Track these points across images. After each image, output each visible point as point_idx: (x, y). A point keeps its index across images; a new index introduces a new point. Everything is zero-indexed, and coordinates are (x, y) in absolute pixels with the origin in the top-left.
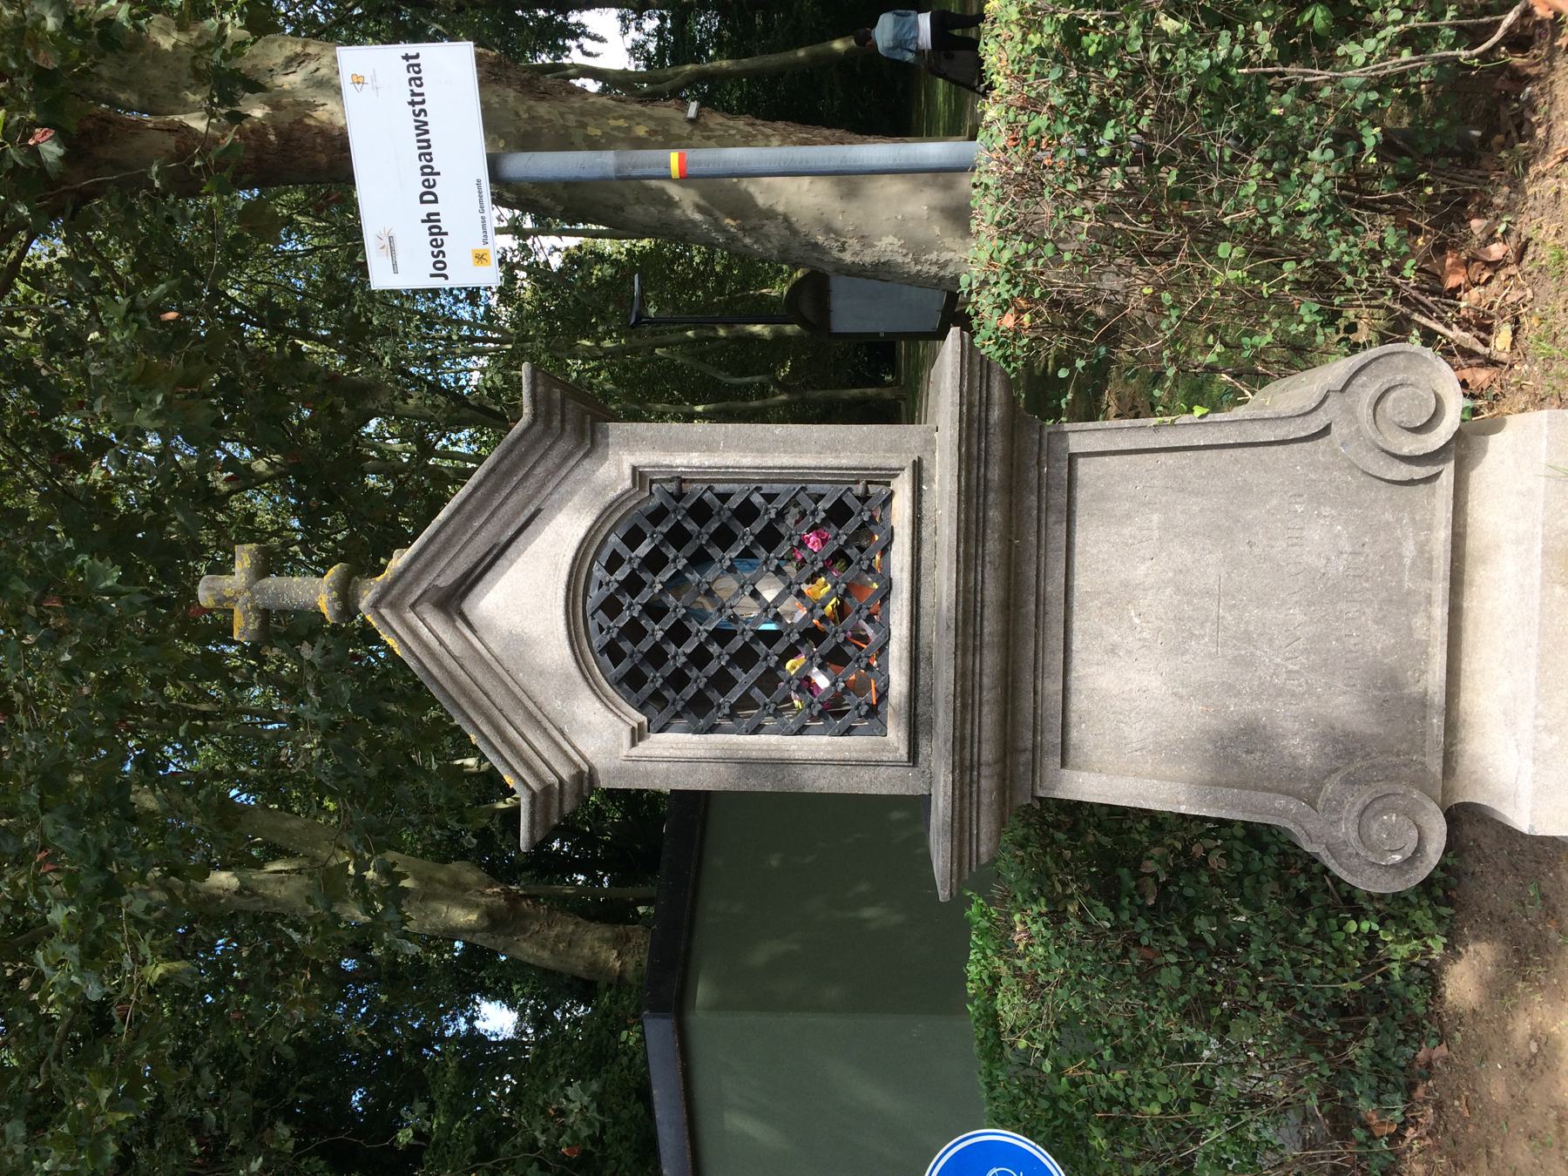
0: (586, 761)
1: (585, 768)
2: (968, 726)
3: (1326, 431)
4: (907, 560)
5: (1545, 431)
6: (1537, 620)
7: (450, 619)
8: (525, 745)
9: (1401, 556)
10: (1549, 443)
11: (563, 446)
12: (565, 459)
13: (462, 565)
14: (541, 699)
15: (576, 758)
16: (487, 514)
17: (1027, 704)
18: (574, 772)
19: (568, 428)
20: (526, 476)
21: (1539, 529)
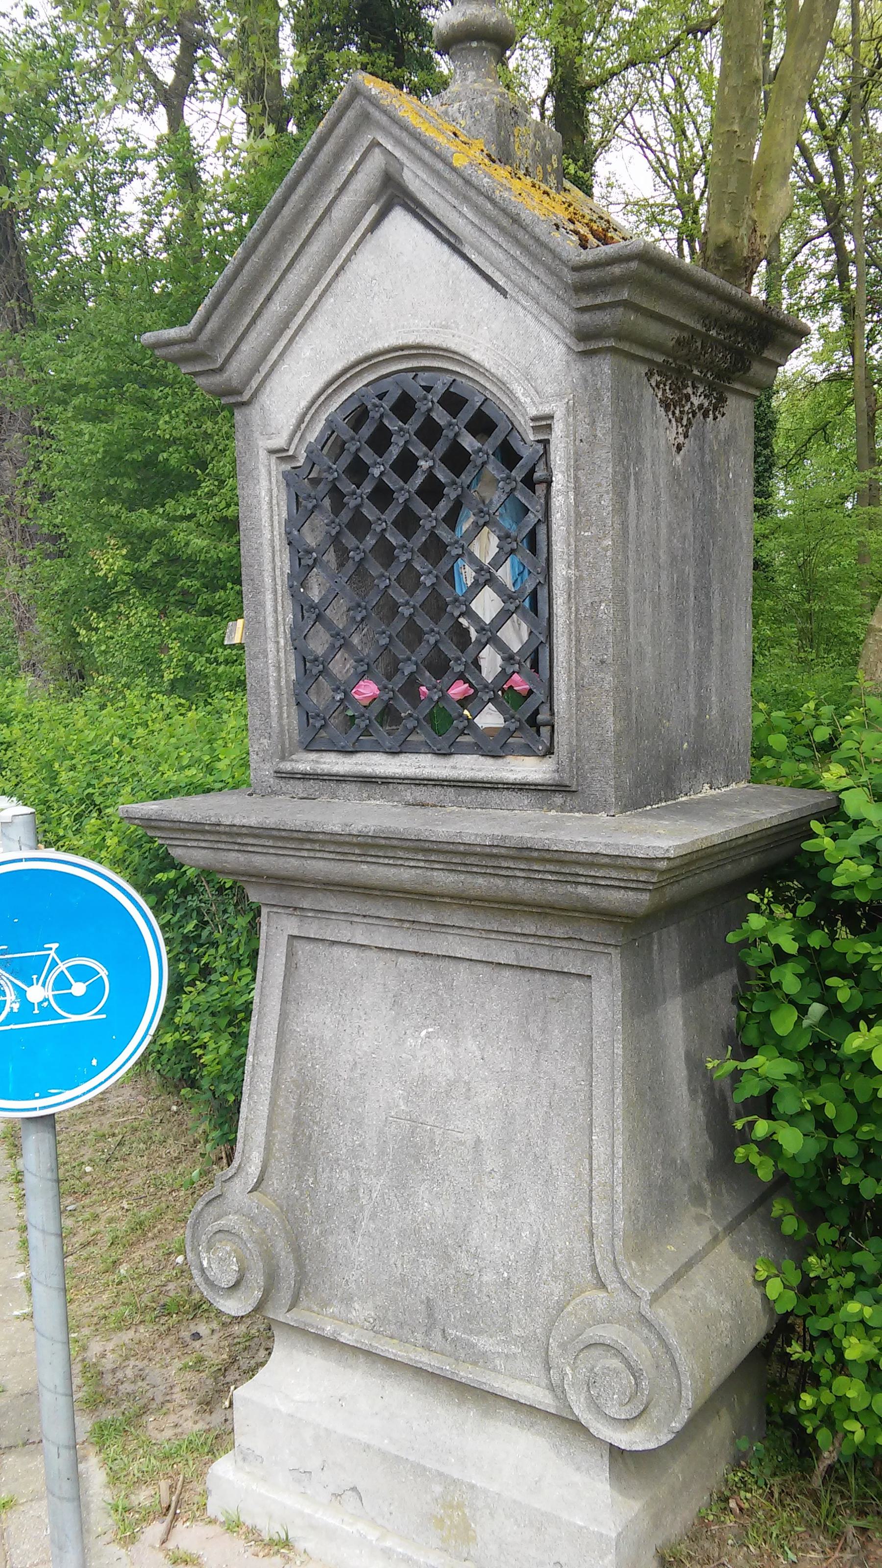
0: (255, 395)
1: (246, 397)
2: (271, 843)
3: (603, 1286)
4: (481, 775)
5: (594, 1528)
6: (411, 1458)
7: (374, 196)
8: (247, 320)
9: (480, 1333)
10: (581, 1528)
11: (565, 312)
12: (555, 318)
13: (428, 198)
14: (310, 329)
15: (254, 384)
16: (477, 221)
17: (331, 903)
18: (751, 373)
19: (586, 317)
20: (524, 268)
21: (494, 1488)
